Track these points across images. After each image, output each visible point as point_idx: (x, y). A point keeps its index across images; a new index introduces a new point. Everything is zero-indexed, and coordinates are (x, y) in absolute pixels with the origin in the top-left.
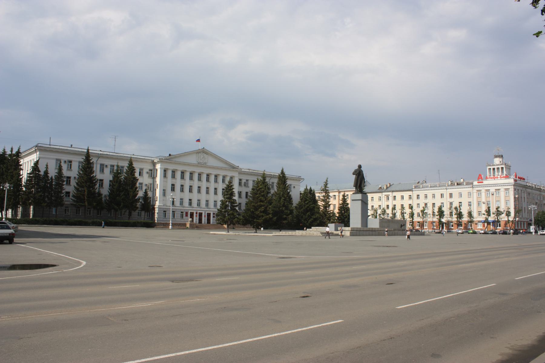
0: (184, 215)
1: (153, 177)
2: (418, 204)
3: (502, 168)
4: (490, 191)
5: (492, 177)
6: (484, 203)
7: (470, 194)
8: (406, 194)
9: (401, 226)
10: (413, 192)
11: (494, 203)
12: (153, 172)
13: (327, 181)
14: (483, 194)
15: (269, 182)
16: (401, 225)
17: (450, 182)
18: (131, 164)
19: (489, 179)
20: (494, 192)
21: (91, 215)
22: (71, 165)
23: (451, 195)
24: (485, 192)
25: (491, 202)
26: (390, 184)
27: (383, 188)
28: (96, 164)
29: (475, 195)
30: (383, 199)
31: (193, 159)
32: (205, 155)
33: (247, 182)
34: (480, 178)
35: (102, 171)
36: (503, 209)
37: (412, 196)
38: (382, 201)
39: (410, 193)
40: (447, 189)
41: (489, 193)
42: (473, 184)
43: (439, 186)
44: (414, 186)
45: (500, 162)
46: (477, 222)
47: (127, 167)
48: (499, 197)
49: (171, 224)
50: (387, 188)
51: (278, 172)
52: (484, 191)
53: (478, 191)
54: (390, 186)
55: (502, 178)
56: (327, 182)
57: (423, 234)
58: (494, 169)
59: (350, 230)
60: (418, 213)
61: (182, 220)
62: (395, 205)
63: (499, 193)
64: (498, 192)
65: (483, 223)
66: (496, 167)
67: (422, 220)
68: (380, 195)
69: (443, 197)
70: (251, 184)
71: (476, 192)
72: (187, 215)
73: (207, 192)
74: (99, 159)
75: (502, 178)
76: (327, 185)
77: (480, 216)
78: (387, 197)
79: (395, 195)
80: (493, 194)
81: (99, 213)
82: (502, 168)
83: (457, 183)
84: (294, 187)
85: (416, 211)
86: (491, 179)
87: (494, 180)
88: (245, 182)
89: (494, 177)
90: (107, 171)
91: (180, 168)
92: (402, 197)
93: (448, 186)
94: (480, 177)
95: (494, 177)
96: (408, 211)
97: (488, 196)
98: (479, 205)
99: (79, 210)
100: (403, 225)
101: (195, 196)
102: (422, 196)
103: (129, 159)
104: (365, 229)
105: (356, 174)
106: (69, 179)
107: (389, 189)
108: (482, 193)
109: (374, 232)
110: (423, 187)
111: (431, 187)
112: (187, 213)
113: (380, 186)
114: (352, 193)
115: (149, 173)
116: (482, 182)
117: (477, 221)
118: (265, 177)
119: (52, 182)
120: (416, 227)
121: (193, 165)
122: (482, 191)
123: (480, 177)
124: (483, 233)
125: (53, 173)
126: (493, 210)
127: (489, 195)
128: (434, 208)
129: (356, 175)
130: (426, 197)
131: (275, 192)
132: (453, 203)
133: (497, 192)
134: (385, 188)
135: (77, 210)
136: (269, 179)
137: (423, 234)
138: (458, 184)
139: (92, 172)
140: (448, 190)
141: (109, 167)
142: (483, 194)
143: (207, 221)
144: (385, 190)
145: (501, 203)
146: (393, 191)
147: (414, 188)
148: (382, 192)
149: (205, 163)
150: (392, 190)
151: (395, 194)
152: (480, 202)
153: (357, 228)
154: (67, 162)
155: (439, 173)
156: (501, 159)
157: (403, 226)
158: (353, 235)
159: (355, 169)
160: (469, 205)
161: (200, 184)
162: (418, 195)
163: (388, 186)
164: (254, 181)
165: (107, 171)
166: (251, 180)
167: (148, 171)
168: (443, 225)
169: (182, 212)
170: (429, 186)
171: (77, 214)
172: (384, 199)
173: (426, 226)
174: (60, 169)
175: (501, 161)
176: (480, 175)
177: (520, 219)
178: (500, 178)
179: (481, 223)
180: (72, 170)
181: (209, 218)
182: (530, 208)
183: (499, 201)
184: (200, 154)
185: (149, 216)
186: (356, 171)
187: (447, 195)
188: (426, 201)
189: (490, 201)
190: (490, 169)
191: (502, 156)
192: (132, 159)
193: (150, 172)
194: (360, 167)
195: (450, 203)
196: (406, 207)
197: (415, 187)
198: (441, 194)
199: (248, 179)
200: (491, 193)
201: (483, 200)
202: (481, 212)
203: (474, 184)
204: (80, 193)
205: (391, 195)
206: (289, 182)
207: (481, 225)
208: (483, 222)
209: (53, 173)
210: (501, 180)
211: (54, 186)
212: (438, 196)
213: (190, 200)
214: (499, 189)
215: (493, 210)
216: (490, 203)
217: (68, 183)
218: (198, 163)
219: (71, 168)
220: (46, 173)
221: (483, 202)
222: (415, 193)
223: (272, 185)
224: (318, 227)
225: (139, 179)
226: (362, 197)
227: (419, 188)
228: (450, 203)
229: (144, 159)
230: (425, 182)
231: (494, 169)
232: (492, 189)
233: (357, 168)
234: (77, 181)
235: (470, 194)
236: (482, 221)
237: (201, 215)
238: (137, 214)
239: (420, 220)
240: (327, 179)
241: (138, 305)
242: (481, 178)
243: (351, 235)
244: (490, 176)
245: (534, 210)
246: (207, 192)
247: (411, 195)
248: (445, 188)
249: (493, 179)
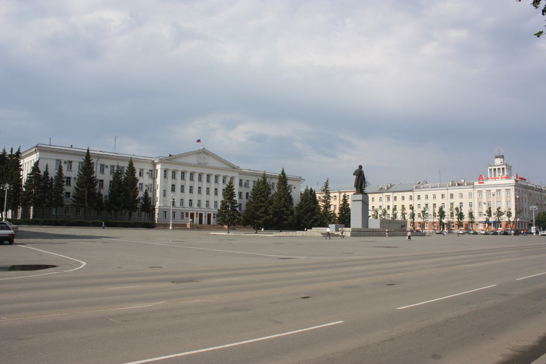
0: (185, 216)
1: (153, 177)
2: (419, 205)
3: (503, 169)
4: (491, 191)
5: (493, 177)
6: (485, 204)
7: (471, 194)
8: (407, 195)
9: (402, 227)
10: (414, 193)
11: (495, 204)
12: (153, 172)
13: (328, 182)
14: (484, 195)
15: (270, 182)
16: (402, 226)
17: (450, 182)
18: (131, 164)
19: (490, 180)
20: (495, 193)
21: (91, 216)
22: (71, 165)
23: (452, 196)
24: (486, 193)
25: (492, 203)
26: (391, 184)
27: (384, 189)
28: (97, 164)
29: (476, 195)
30: (384, 199)
31: (193, 160)
32: (205, 155)
33: (247, 183)
34: (481, 179)
35: (102, 171)
36: (504, 209)
37: (413, 197)
38: (383, 202)
39: (411, 194)
40: (448, 190)
41: (490, 194)
42: (474, 184)
43: (440, 187)
44: (414, 186)
45: (501, 162)
46: (478, 222)
48: (500, 197)
49: (171, 225)
50: (388, 188)
51: (278, 173)
52: (485, 192)
53: (479, 192)
54: (391, 186)
55: (503, 179)
56: (328, 183)
57: (424, 235)
58: (495, 169)
59: (351, 230)
60: (419, 214)
61: (182, 221)
62: (396, 206)
63: (500, 193)
64: (498, 192)
65: (484, 223)
66: (497, 168)
67: (423, 221)
68: (380, 195)
69: (444, 198)
70: (251, 185)
71: (477, 193)
72: (187, 216)
73: (208, 193)
74: (99, 159)
75: (503, 178)
76: (327, 185)
77: (481, 217)
78: (388, 197)
79: (395, 196)
80: (494, 194)
82: (503, 169)
83: (458, 184)
84: (295, 188)
85: (417, 211)
86: (492, 180)
87: (495, 180)
88: (245, 183)
89: (495, 177)
90: (107, 171)
91: (181, 169)
92: (403, 198)
93: (449, 186)
94: (481, 178)
95: (495, 177)
96: (408, 211)
97: (489, 197)
98: (480, 206)
99: (79, 211)
100: (403, 225)
101: (195, 197)
102: (423, 197)
103: (129, 159)
104: (366, 229)
105: (357, 174)
106: (69, 180)
107: (390, 190)
108: (483, 193)
109: (374, 233)
110: (423, 188)
111: (432, 187)
112: (187, 214)
113: (381, 187)
114: (352, 193)
115: (149, 173)
116: (483, 183)
117: (478, 221)
118: (266, 178)
119: (52, 182)
120: (417, 227)
121: (194, 166)
122: (483, 192)
123: (481, 178)
124: (484, 234)
125: (53, 173)
126: (494, 210)
127: (490, 196)
129: (357, 176)
130: (427, 197)
131: (276, 192)
132: (454, 204)
133: (498, 193)
134: (386, 188)
135: (77, 210)
136: (270, 179)
137: (424, 235)
138: (458, 185)
139: (92, 172)
140: (449, 191)
141: (109, 167)
142: (484, 195)
143: (207, 221)
144: (386, 191)
145: (502, 204)
146: (394, 192)
147: (414, 188)
148: (383, 193)
149: (206, 164)
150: (393, 190)
151: (395, 194)
152: (481, 202)
153: (358, 229)
154: (67, 162)
155: (440, 174)
156: (502, 160)
157: (403, 226)
158: (354, 236)
159: (356, 169)
161: (200, 184)
162: (419, 196)
163: (389, 186)
164: (254, 182)
165: (107, 171)
166: (251, 181)
167: (148, 171)
168: (444, 225)
169: (182, 213)
170: (430, 186)
171: (77, 214)
172: (385, 199)
173: (426, 227)
174: (60, 169)
175: (502, 162)
176: (481, 176)
178: (501, 178)
179: (482, 224)
180: (72, 170)
181: (210, 219)
182: (531, 208)
183: (500, 202)
184: (200, 154)
185: (150, 217)
186: (356, 171)
187: (447, 196)
188: (427, 202)
189: (491, 202)
190: (491, 169)
191: (503, 157)
192: (132, 159)
193: (150, 173)
194: (361, 167)
195: (451, 203)
196: (407, 207)
197: (416, 188)
198: (442, 195)
199: (248, 179)
200: (492, 193)
201: (484, 200)
202: (482, 212)
203: (475, 185)
204: (80, 193)
205: (392, 196)
206: (289, 183)
207: (482, 225)
208: (484, 222)
209: (53, 173)
210: (502, 181)
211: (54, 187)
212: (439, 196)
213: (190, 200)
214: (500, 190)
215: (494, 210)
216: (491, 203)
217: (69, 183)
218: (198, 163)
219: (71, 168)
220: (46, 173)
221: (484, 203)
222: (416, 194)
223: (272, 186)
224: (318, 228)
225: (139, 180)
226: (363, 197)
227: (420, 188)
228: (451, 203)
229: (144, 159)
230: (426, 182)
231: (495, 169)
232: (493, 190)
233: (357, 168)
234: (77, 182)
235: (470, 195)
236: (483, 221)
237: (201, 215)
238: (138, 215)
239: (421, 220)
240: (328, 179)
242: (482, 178)
243: (351, 236)
244: (491, 176)
245: (535, 211)
246: (208, 193)
247: (412, 196)
248: (446, 188)
249: (494, 180)
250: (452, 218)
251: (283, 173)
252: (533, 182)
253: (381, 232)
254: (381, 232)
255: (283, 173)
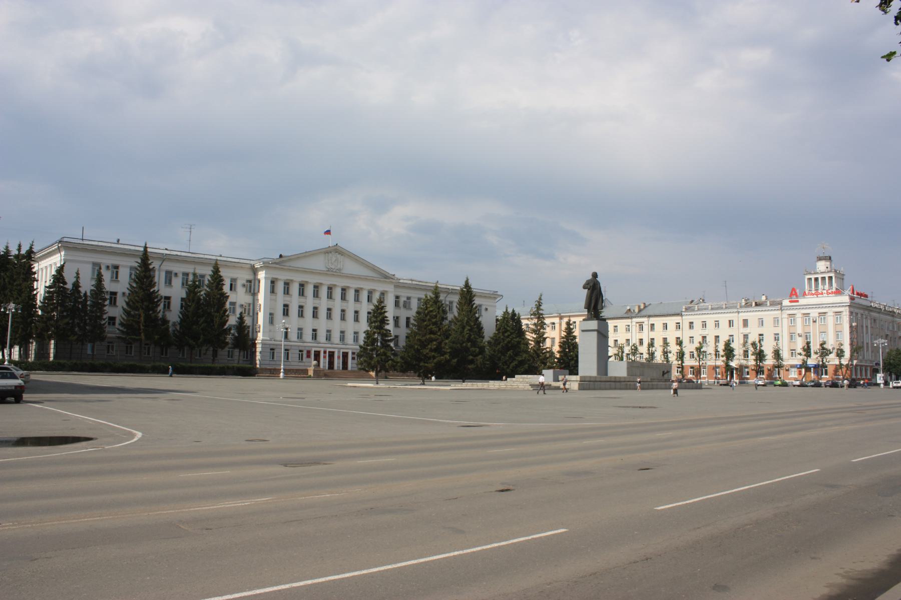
0: (305, 356)
1: (252, 292)
2: (691, 337)
3: (830, 278)
4: (811, 315)
5: (813, 292)
6: (800, 336)
7: (778, 320)
8: (671, 321)
9: (664, 373)
10: (683, 317)
11: (817, 336)
12: (253, 284)
13: (541, 300)
14: (799, 321)
15: (445, 300)
16: (663, 372)
17: (743, 301)
19: (809, 296)
20: (817, 318)
23: (745, 323)
24: (802, 318)
25: (811, 334)
26: (644, 304)
27: (634, 311)
29: (786, 322)
30: (634, 328)
31: (318, 264)
32: (339, 256)
33: (408, 301)
34: (794, 295)
36: (832, 345)
37: (681, 324)
38: (632, 332)
39: (677, 319)
40: (739, 312)
41: (809, 319)
42: (782, 304)
43: (726, 308)
44: (684, 307)
45: (827, 268)
46: (789, 367)
47: (210, 275)
48: (826, 325)
50: (640, 311)
51: (459, 284)
52: (801, 316)
53: (790, 316)
54: (645, 307)
55: (830, 295)
57: (699, 387)
58: (816, 279)
59: (579, 380)
60: (691, 352)
61: (300, 364)
62: (653, 339)
63: (824, 318)
64: (823, 317)
65: (798, 368)
66: (819, 276)
67: (698, 364)
68: (628, 322)
69: (733, 326)
70: (414, 305)
71: (788, 318)
72: (309, 356)
73: (343, 318)
74: (164, 262)
75: (830, 293)
76: (540, 305)
77: (794, 357)
78: (640, 325)
79: (652, 323)
80: (815, 320)
81: (164, 353)
82: (830, 278)
83: (756, 303)
84: (486, 309)
85: (688, 348)
86: (811, 296)
87: (817, 297)
88: (404, 301)
89: (817, 292)
92: (665, 326)
93: (741, 307)
94: (794, 293)
95: (817, 292)
96: (674, 348)
97: (807, 324)
98: (792, 339)
100: (666, 371)
102: (698, 325)
103: (214, 262)
104: (604, 378)
105: (589, 287)
107: (643, 313)
108: (797, 319)
109: (618, 384)
110: (699, 310)
111: (712, 309)
112: (309, 352)
113: (628, 308)
115: (246, 286)
116: (797, 301)
117: (789, 365)
118: (439, 293)
120: (688, 375)
121: (320, 273)
122: (797, 316)
123: (794, 293)
124: (798, 386)
126: (815, 347)
127: (809, 322)
128: (717, 344)
129: (589, 289)
130: (704, 325)
131: (455, 317)
132: (750, 336)
133: (821, 318)
134: (637, 310)
136: (445, 295)
137: (699, 387)
138: (757, 305)
140: (740, 314)
142: (799, 321)
143: (342, 365)
144: (637, 314)
145: (828, 335)
146: (649, 316)
147: (684, 310)
148: (631, 318)
149: (340, 270)
150: (649, 314)
151: (652, 320)
152: (794, 333)
153: (590, 377)
155: (726, 286)
156: (828, 263)
157: (666, 373)
158: (584, 389)
160: (775, 340)
161: (330, 304)
162: (691, 323)
163: (642, 307)
164: (419, 299)
166: (415, 298)
167: (244, 282)
168: (733, 372)
170: (710, 307)
172: (635, 328)
173: (704, 374)
175: (829, 266)
176: (794, 289)
177: (860, 362)
178: (827, 294)
179: (796, 369)
181: (346, 361)
182: (876, 343)
183: (825, 332)
184: (330, 255)
185: (247, 358)
186: (588, 283)
187: (738, 323)
188: (704, 333)
189: (810, 333)
190: (810, 279)
191: (830, 258)
192: (219, 262)
193: (247, 285)
194: (595, 275)
195: (744, 335)
196: (672, 342)
197: (687, 309)
198: (730, 321)
199: (409, 295)
200: (811, 318)
201: (799, 330)
202: (795, 350)
203: (783, 305)
204: (132, 319)
205: (646, 323)
206: (477, 301)
207: (795, 372)
208: (798, 367)
210: (828, 298)
212: (724, 324)
213: (314, 330)
214: (825, 313)
215: (815, 347)
216: (810, 335)
218: (327, 270)
221: (799, 334)
222: (686, 320)
223: (449, 306)
224: (525, 376)
226: (599, 325)
227: (693, 310)
228: (744, 335)
229: (238, 263)
230: (703, 300)
231: (816, 279)
232: (814, 313)
233: (590, 277)
235: (776, 321)
236: (797, 365)
237: (331, 355)
239: (694, 363)
242: (796, 294)
243: (579, 389)
246: (343, 318)
247: (679, 323)
248: (735, 310)
249: (816, 296)
250: (745, 359)
251: (467, 285)
252: (880, 300)
253: (629, 382)
254: (629, 382)
255: (467, 285)
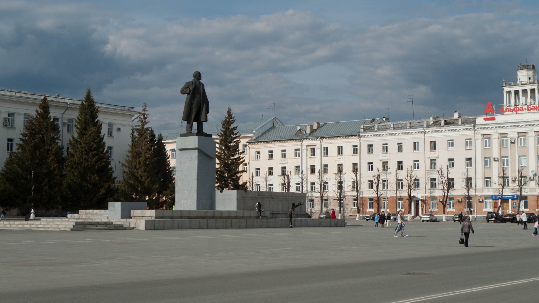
2: (369, 163)
3: (533, 91)
4: (509, 136)
5: (512, 108)
6: (496, 160)
7: (471, 142)
8: (347, 143)
9: (294, 206)
10: (362, 139)
11: (515, 159)
14: (495, 143)
15: (62, 118)
16: (293, 204)
17: (431, 118)
19: (507, 113)
20: (516, 139)
23: (433, 146)
25: (509, 158)
26: (318, 123)
27: (305, 132)
29: (479, 144)
30: (304, 152)
33: (10, 118)
36: (532, 171)
37: (358, 148)
38: (302, 158)
39: (354, 141)
40: (425, 133)
41: (507, 141)
42: (476, 122)
43: (411, 127)
44: (362, 127)
45: (530, 78)
46: (483, 198)
48: (526, 148)
50: (312, 131)
53: (485, 136)
54: (319, 127)
55: (532, 111)
57: (342, 224)
58: (517, 93)
59: (154, 216)
60: (369, 181)
62: (326, 166)
63: (525, 139)
64: (522, 138)
65: (493, 199)
66: (520, 89)
68: (297, 144)
70: (20, 124)
75: (531, 109)
76: (145, 118)
77: (489, 187)
78: (311, 149)
79: (326, 146)
80: (513, 141)
82: (533, 91)
83: (445, 121)
84: (119, 129)
85: (366, 176)
86: (509, 113)
88: (5, 118)
89: (517, 108)
92: (340, 150)
93: (428, 126)
95: (517, 108)
96: (348, 178)
97: (505, 147)
98: (486, 165)
100: (297, 204)
102: (377, 148)
104: (210, 213)
105: (188, 91)
107: (316, 133)
108: (530, 138)
109: (212, 221)
110: (379, 130)
111: (395, 129)
113: (298, 128)
117: (483, 196)
118: (48, 107)
120: (367, 209)
124: (427, 221)
126: (512, 173)
127: (507, 145)
129: (188, 94)
130: (400, 147)
131: (73, 138)
133: (521, 139)
134: (308, 131)
136: (62, 111)
137: (342, 224)
138: (446, 123)
140: (427, 135)
142: (495, 143)
144: (308, 136)
145: (528, 160)
146: (322, 138)
147: (362, 130)
148: (301, 140)
150: (322, 136)
151: (326, 143)
153: (190, 211)
155: (412, 102)
156: (531, 73)
157: (297, 206)
158: (155, 229)
162: (370, 146)
163: (315, 127)
164: (26, 116)
168: (418, 204)
170: (392, 126)
172: (305, 153)
175: (532, 77)
178: (528, 110)
179: (491, 201)
183: (525, 156)
186: (187, 86)
187: (425, 146)
188: (385, 157)
189: (507, 157)
190: (509, 92)
191: (533, 66)
194: (198, 76)
195: (431, 160)
196: (347, 168)
197: (365, 130)
198: (415, 143)
199: (11, 111)
201: (495, 154)
202: (490, 178)
203: (477, 123)
205: (318, 146)
206: (101, 118)
207: (490, 203)
208: (494, 198)
212: (408, 147)
214: (525, 133)
215: (512, 173)
216: (507, 161)
221: (494, 158)
222: (366, 140)
223: (68, 125)
224: (91, 211)
226: (199, 142)
227: (373, 130)
228: (431, 160)
230: (387, 119)
231: (517, 93)
232: (512, 133)
233: (191, 79)
235: (468, 142)
236: (492, 196)
239: (372, 194)
241: (452, 293)
243: (147, 229)
247: (356, 146)
248: (421, 130)
249: (515, 112)
